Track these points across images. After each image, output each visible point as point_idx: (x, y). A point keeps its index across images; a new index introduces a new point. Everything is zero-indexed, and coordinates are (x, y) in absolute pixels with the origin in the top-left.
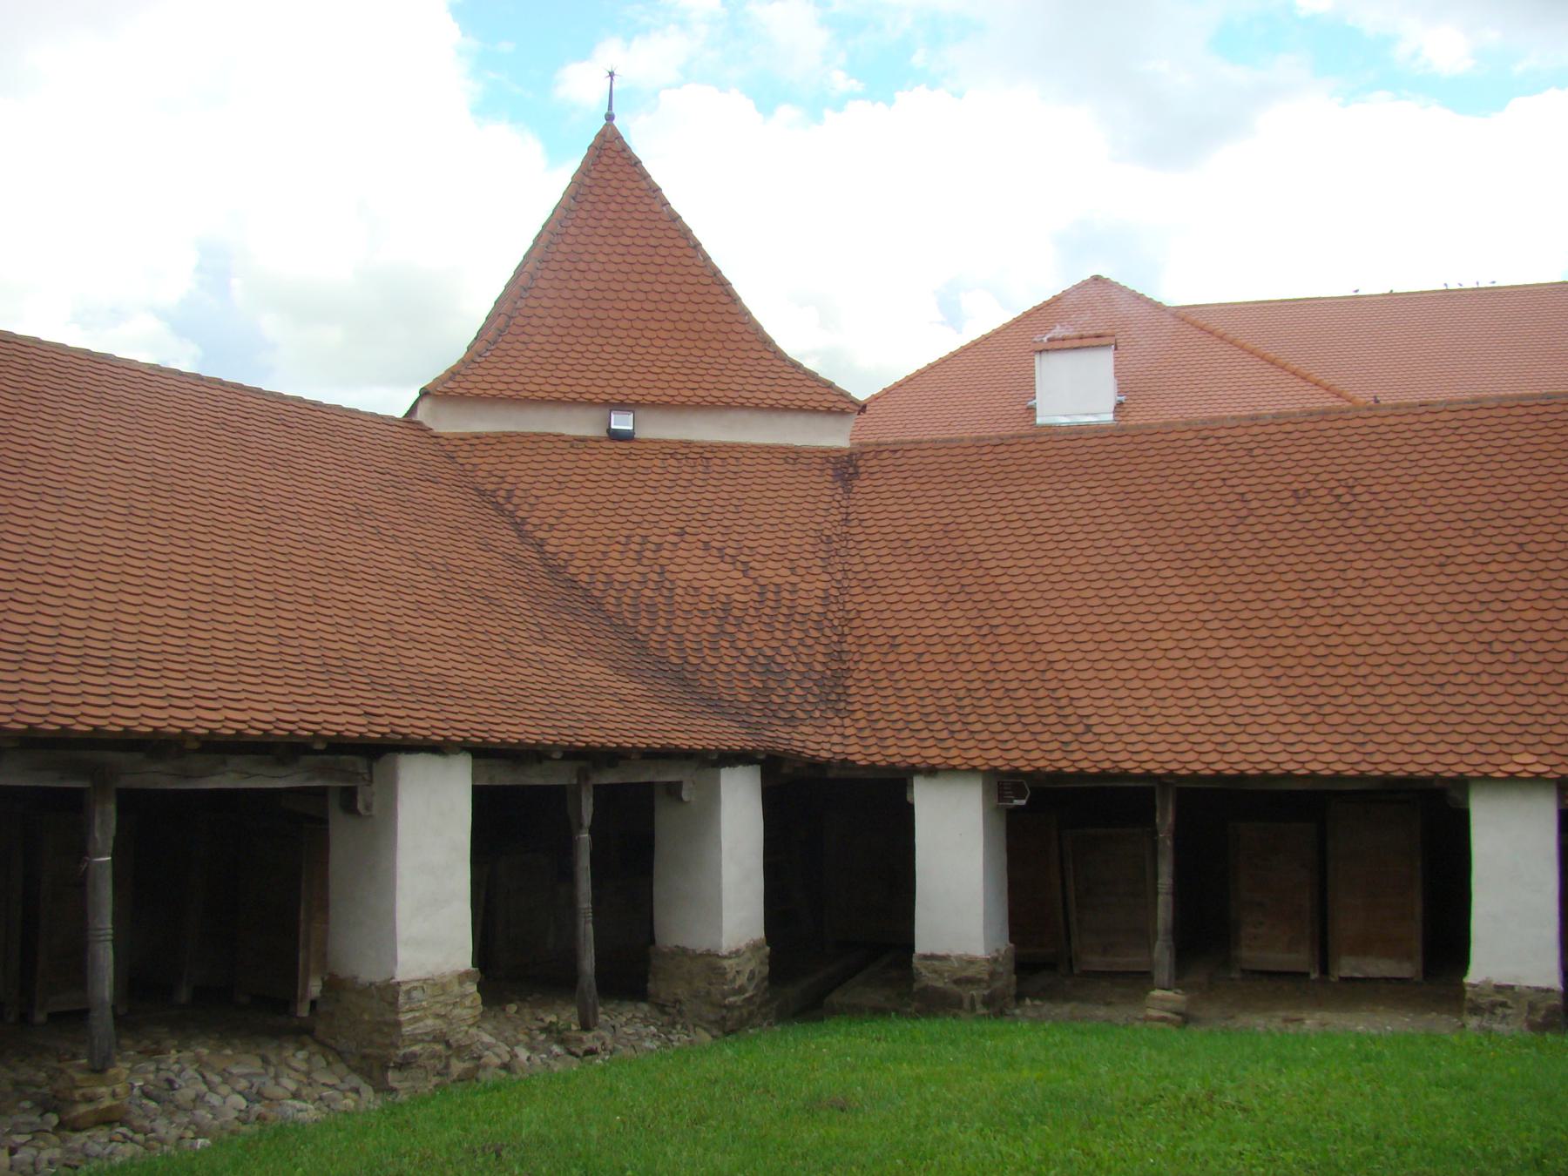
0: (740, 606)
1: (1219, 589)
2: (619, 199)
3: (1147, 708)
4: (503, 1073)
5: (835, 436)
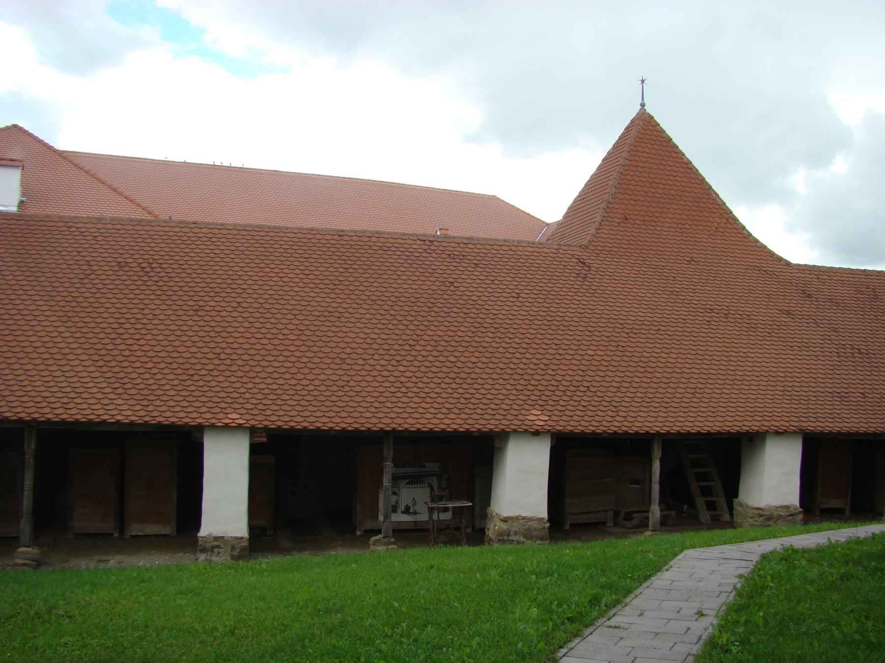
1: (70, 314)
3: (22, 381)
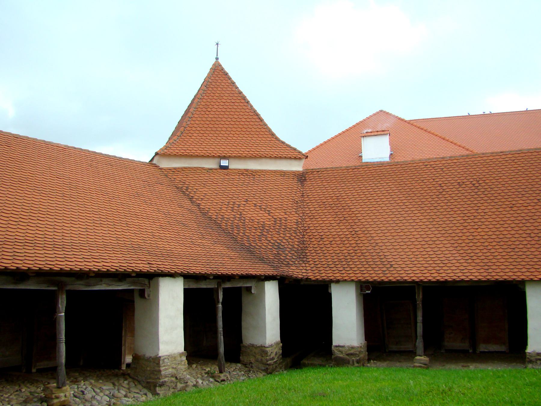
0: (268, 225)
1: (434, 217)
2: (221, 86)
4: (194, 388)
5: (297, 167)
